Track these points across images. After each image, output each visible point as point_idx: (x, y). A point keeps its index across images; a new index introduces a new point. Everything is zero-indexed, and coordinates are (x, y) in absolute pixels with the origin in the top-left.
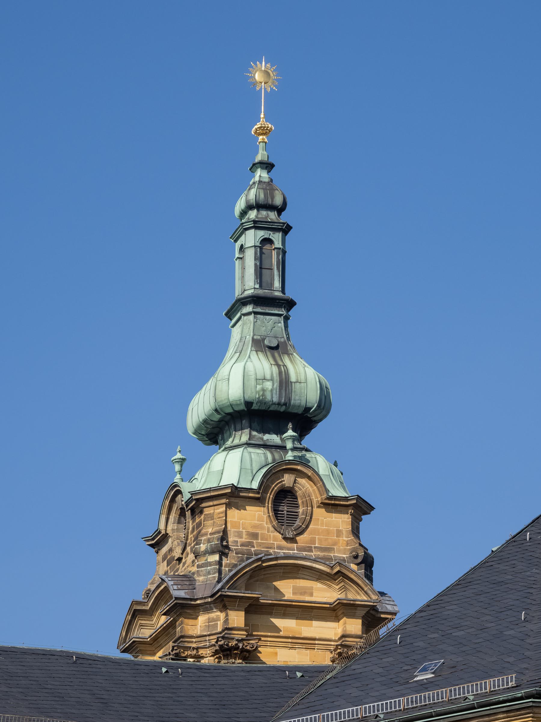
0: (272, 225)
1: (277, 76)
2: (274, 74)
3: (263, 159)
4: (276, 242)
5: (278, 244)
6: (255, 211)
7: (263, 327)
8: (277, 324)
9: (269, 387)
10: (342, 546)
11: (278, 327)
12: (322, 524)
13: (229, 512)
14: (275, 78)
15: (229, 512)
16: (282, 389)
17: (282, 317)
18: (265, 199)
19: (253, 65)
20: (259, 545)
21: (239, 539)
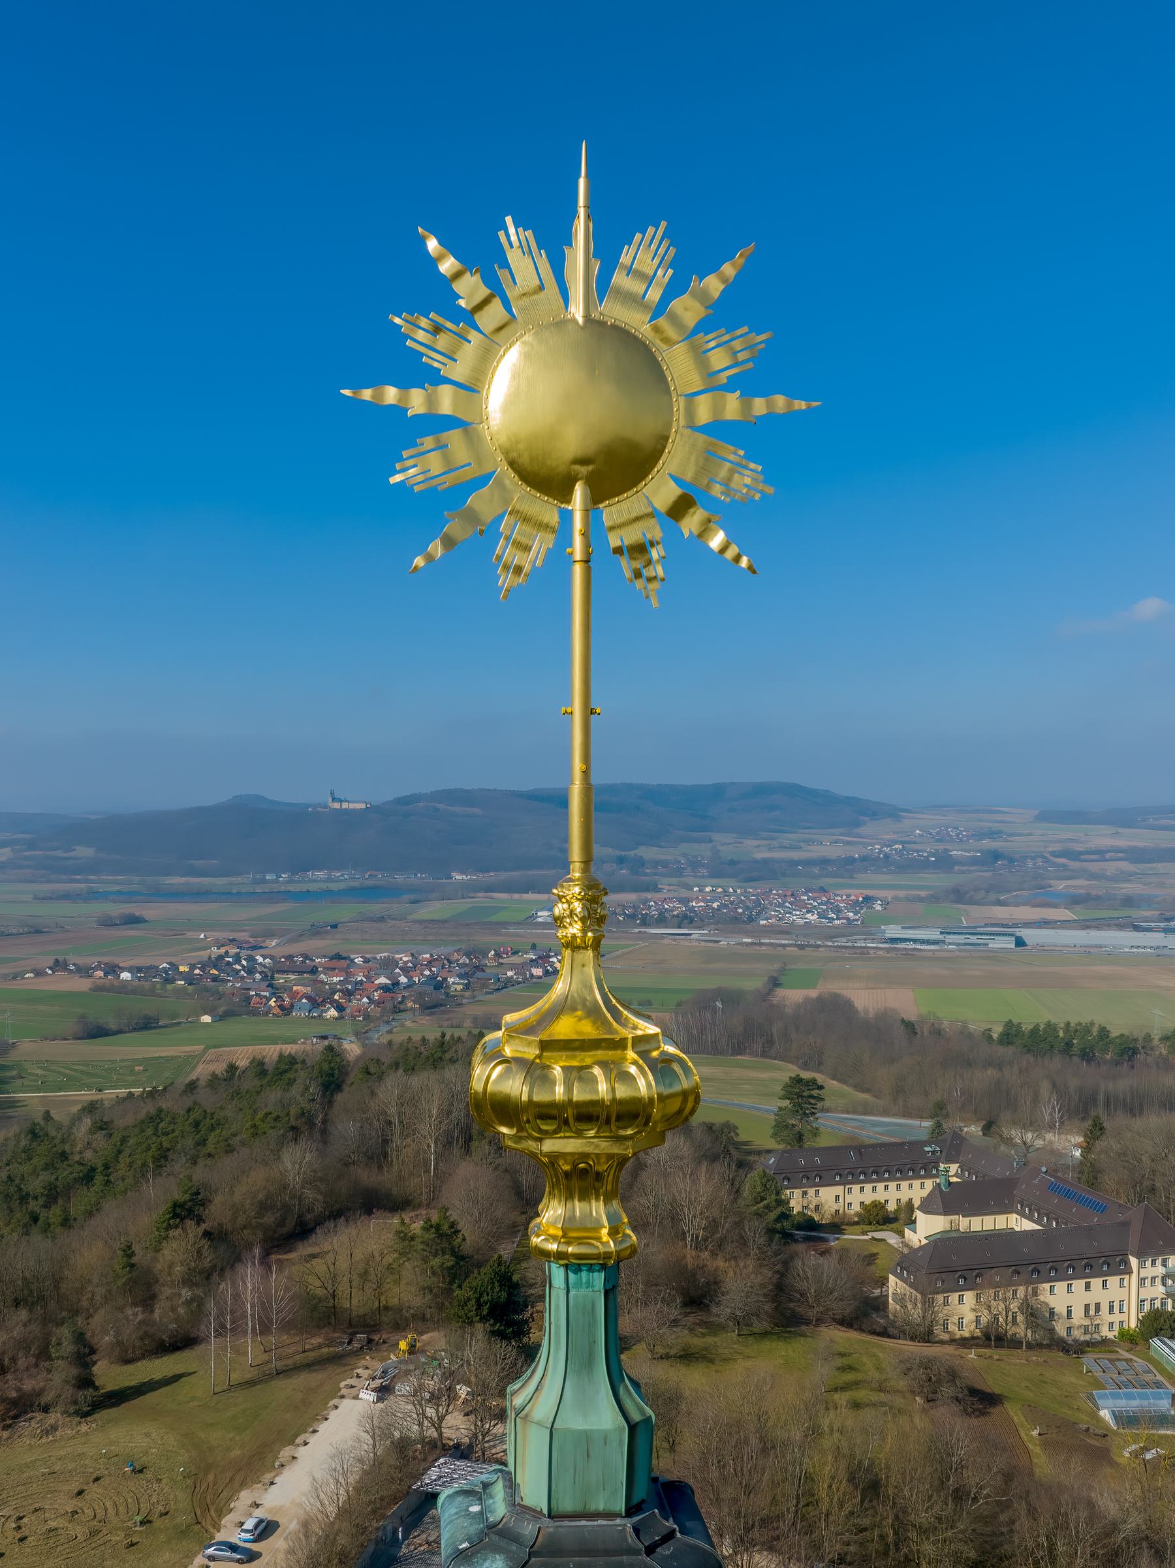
14: (732, 406)
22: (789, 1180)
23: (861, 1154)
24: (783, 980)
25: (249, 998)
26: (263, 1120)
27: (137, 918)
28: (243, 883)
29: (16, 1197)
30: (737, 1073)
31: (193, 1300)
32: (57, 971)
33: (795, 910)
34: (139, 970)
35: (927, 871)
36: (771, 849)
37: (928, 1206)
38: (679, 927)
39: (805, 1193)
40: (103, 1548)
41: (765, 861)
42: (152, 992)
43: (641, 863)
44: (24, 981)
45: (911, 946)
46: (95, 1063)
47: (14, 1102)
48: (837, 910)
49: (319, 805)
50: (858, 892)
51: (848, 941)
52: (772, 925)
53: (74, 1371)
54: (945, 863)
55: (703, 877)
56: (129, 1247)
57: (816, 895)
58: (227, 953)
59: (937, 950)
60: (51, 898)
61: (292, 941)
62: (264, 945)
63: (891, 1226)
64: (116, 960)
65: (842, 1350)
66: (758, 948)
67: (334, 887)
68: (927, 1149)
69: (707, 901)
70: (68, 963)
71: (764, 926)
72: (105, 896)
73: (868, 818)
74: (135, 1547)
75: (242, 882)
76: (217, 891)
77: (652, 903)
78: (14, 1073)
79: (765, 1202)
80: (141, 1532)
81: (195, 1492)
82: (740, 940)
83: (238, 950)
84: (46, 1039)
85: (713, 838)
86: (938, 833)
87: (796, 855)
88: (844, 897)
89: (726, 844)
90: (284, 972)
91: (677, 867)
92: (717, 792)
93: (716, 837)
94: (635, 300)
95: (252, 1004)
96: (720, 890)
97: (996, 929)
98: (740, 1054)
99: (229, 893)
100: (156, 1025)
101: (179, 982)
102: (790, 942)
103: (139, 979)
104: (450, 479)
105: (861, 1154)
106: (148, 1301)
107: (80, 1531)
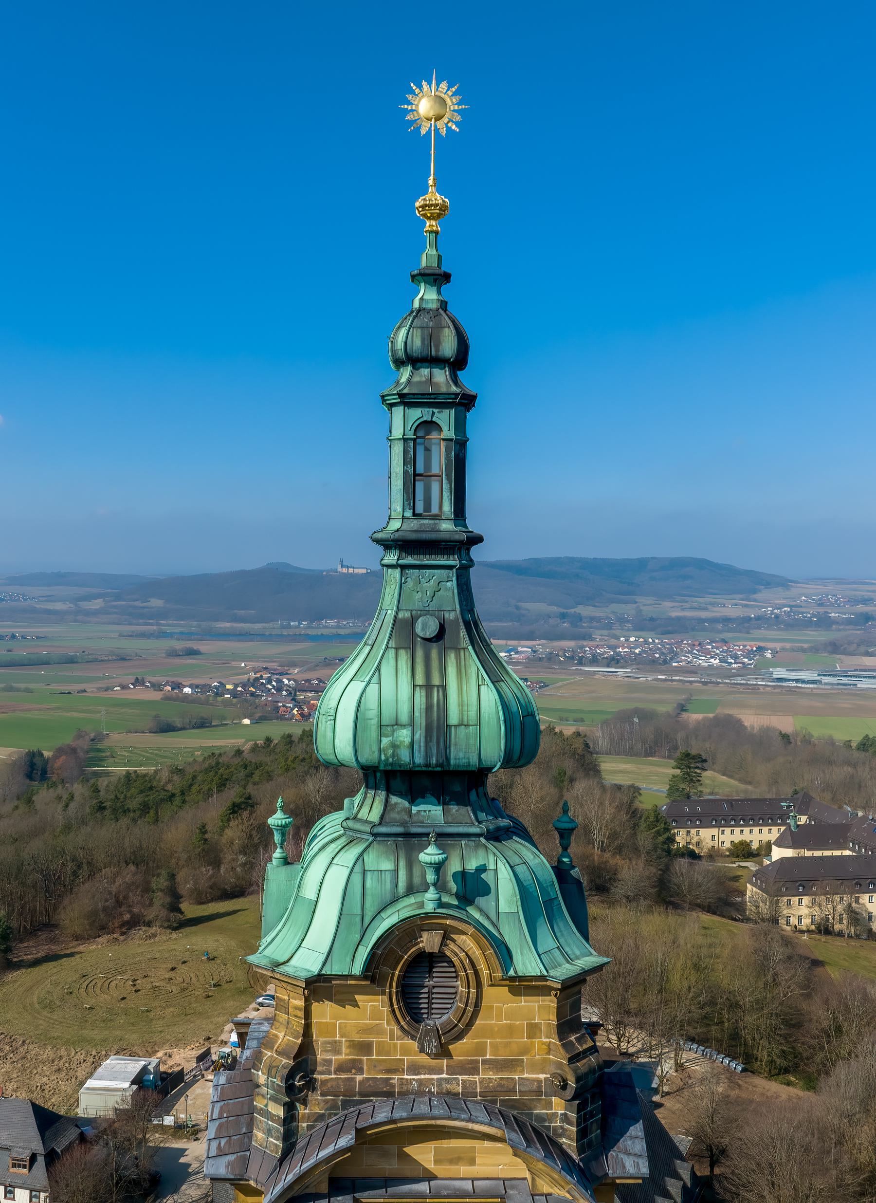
0: (434, 399)
1: (458, 104)
2: (454, 100)
3: (429, 265)
4: (445, 428)
5: (448, 432)
6: (409, 368)
7: (418, 592)
8: (443, 583)
9: (405, 740)
10: (539, 1055)
11: (446, 589)
12: (499, 1017)
13: (315, 1006)
14: (456, 108)
15: (315, 1006)
16: (431, 741)
17: (454, 570)
18: (423, 348)
19: (414, 88)
20: (374, 1065)
21: (332, 1056)
22: (677, 822)
23: (732, 805)
24: (688, 706)
25: (278, 708)
26: (293, 762)
27: (195, 651)
28: (274, 628)
29: (120, 810)
30: (648, 769)
31: (246, 863)
32: (137, 686)
33: (701, 656)
34: (197, 687)
35: (809, 629)
36: (683, 610)
37: (780, 843)
38: (608, 666)
39: (688, 832)
40: (190, 997)
41: (679, 619)
42: (207, 702)
43: (580, 618)
44: (113, 692)
45: (794, 684)
46: (165, 749)
47: (108, 773)
48: (735, 657)
49: (331, 570)
50: (753, 643)
51: (743, 679)
52: (681, 667)
53: (168, 900)
54: (824, 622)
55: (628, 630)
56: (204, 827)
57: (718, 645)
58: (261, 676)
59: (815, 688)
60: (132, 636)
61: (310, 670)
62: (289, 672)
63: (754, 859)
64: (180, 680)
65: (707, 926)
66: (670, 683)
67: (342, 632)
68: (783, 804)
69: (630, 648)
70: (145, 681)
71: (675, 667)
72: (171, 636)
73: (763, 587)
74: (211, 998)
75: (272, 628)
76: (254, 633)
77: (587, 649)
78: (108, 754)
79: (656, 829)
80: (214, 990)
81: (250, 972)
82: (656, 677)
83: (270, 675)
84: (130, 732)
85: (637, 600)
86: (820, 599)
87: (703, 614)
88: (741, 647)
89: (648, 605)
90: (303, 691)
91: (608, 622)
92: (641, 564)
93: (640, 599)
94: (442, 92)
95: (280, 712)
96: (641, 640)
97: (864, 673)
98: (652, 756)
99: (262, 635)
100: (209, 725)
101: (226, 696)
102: (696, 679)
103: (197, 693)
104: (414, 119)
105: (732, 805)
106: (216, 863)
107: (174, 989)
